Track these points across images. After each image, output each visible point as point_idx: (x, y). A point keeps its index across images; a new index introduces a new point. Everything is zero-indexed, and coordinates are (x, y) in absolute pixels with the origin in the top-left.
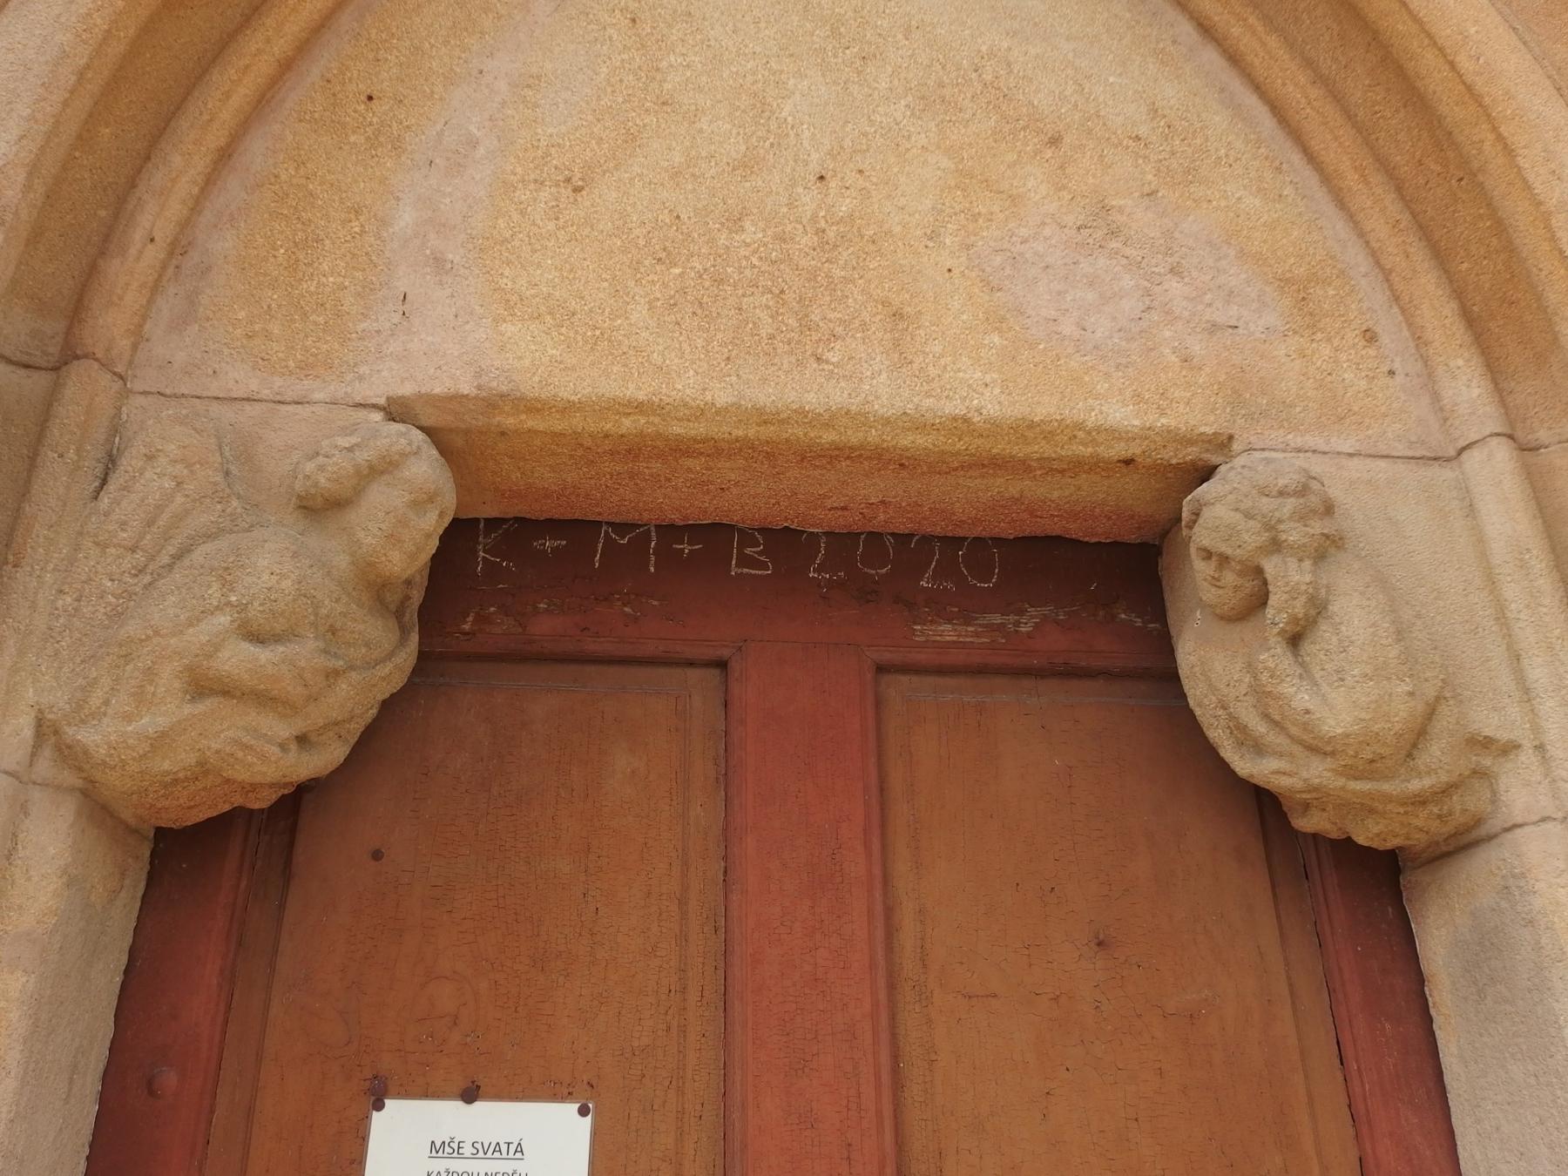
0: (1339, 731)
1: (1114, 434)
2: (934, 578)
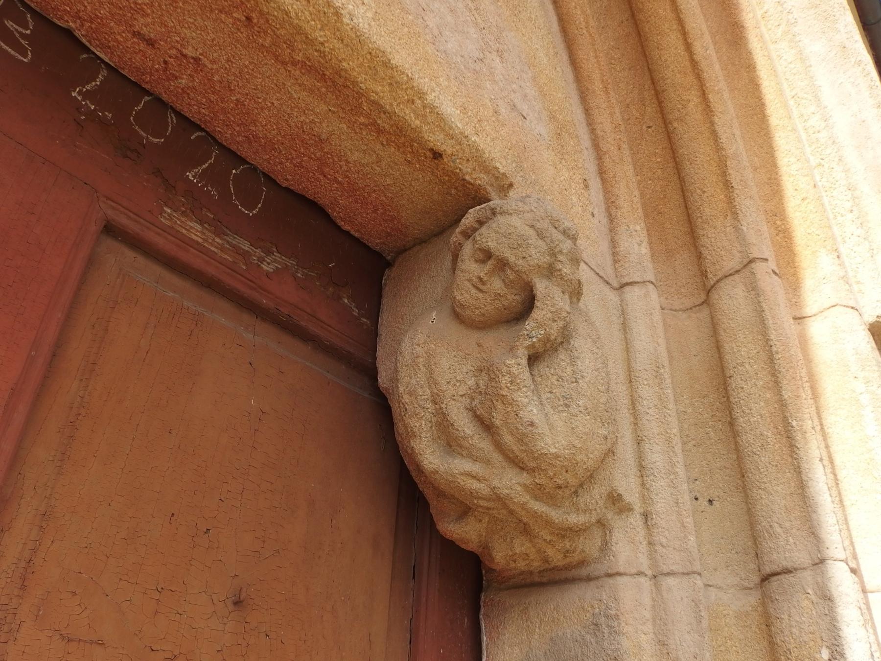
0: (553, 450)
2: (202, 176)
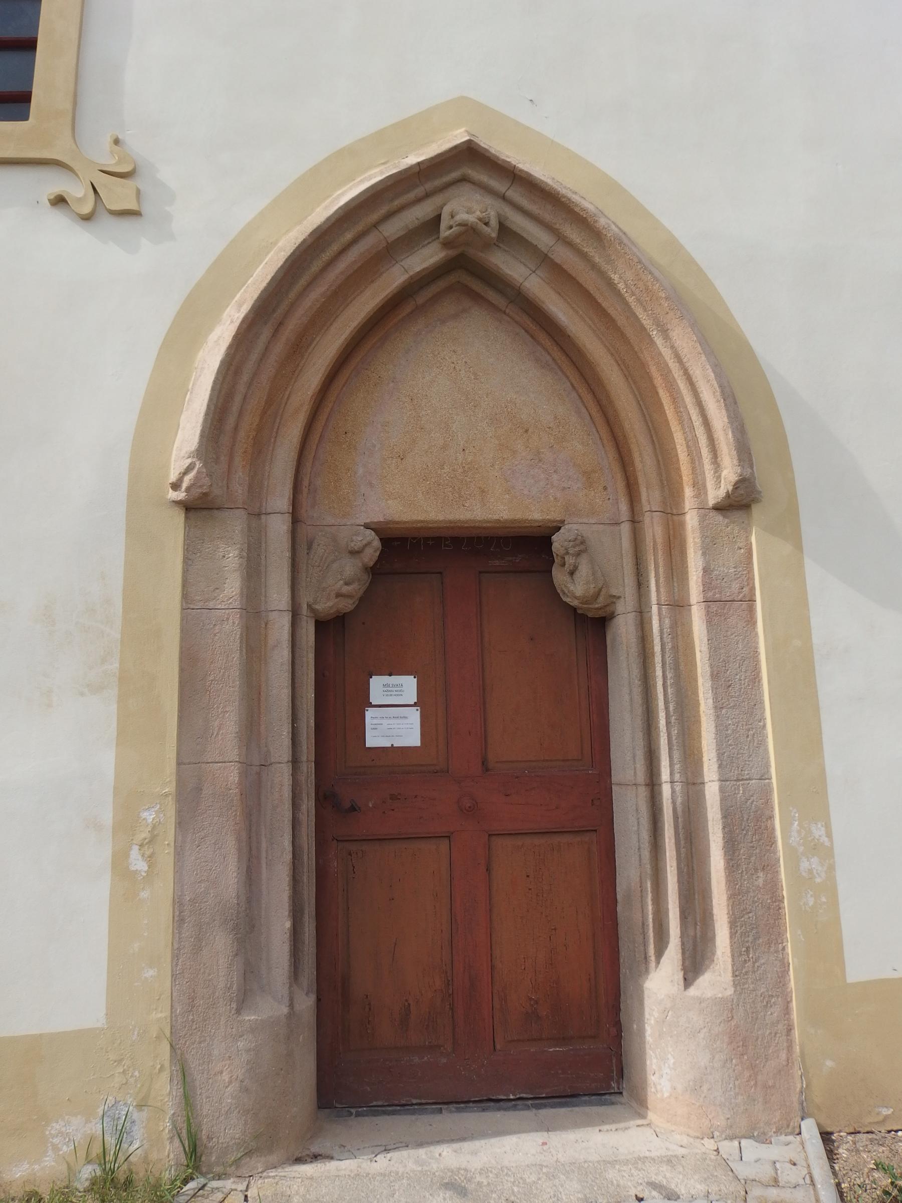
1: (536, 521)
